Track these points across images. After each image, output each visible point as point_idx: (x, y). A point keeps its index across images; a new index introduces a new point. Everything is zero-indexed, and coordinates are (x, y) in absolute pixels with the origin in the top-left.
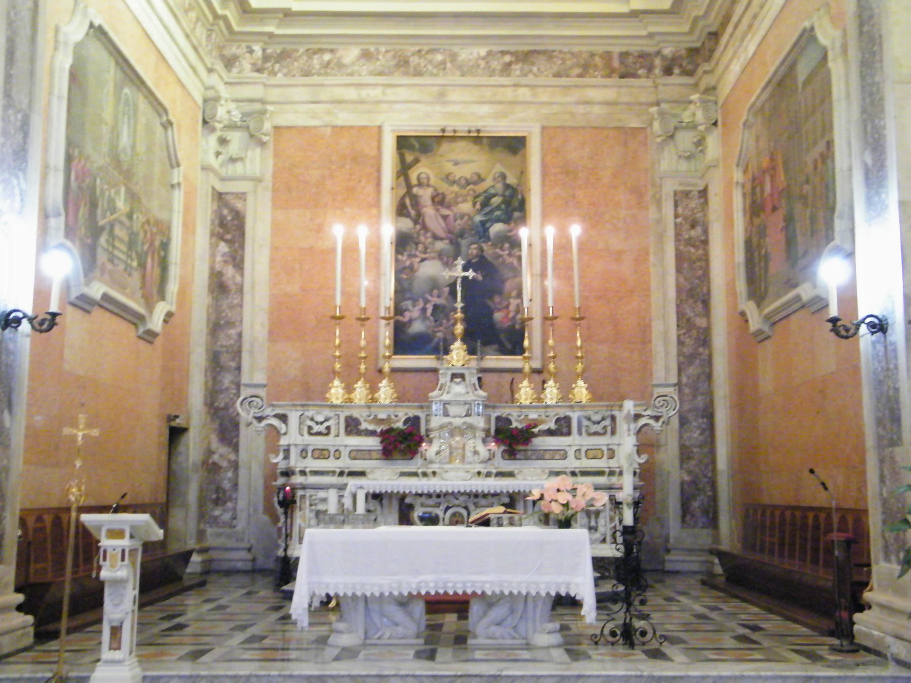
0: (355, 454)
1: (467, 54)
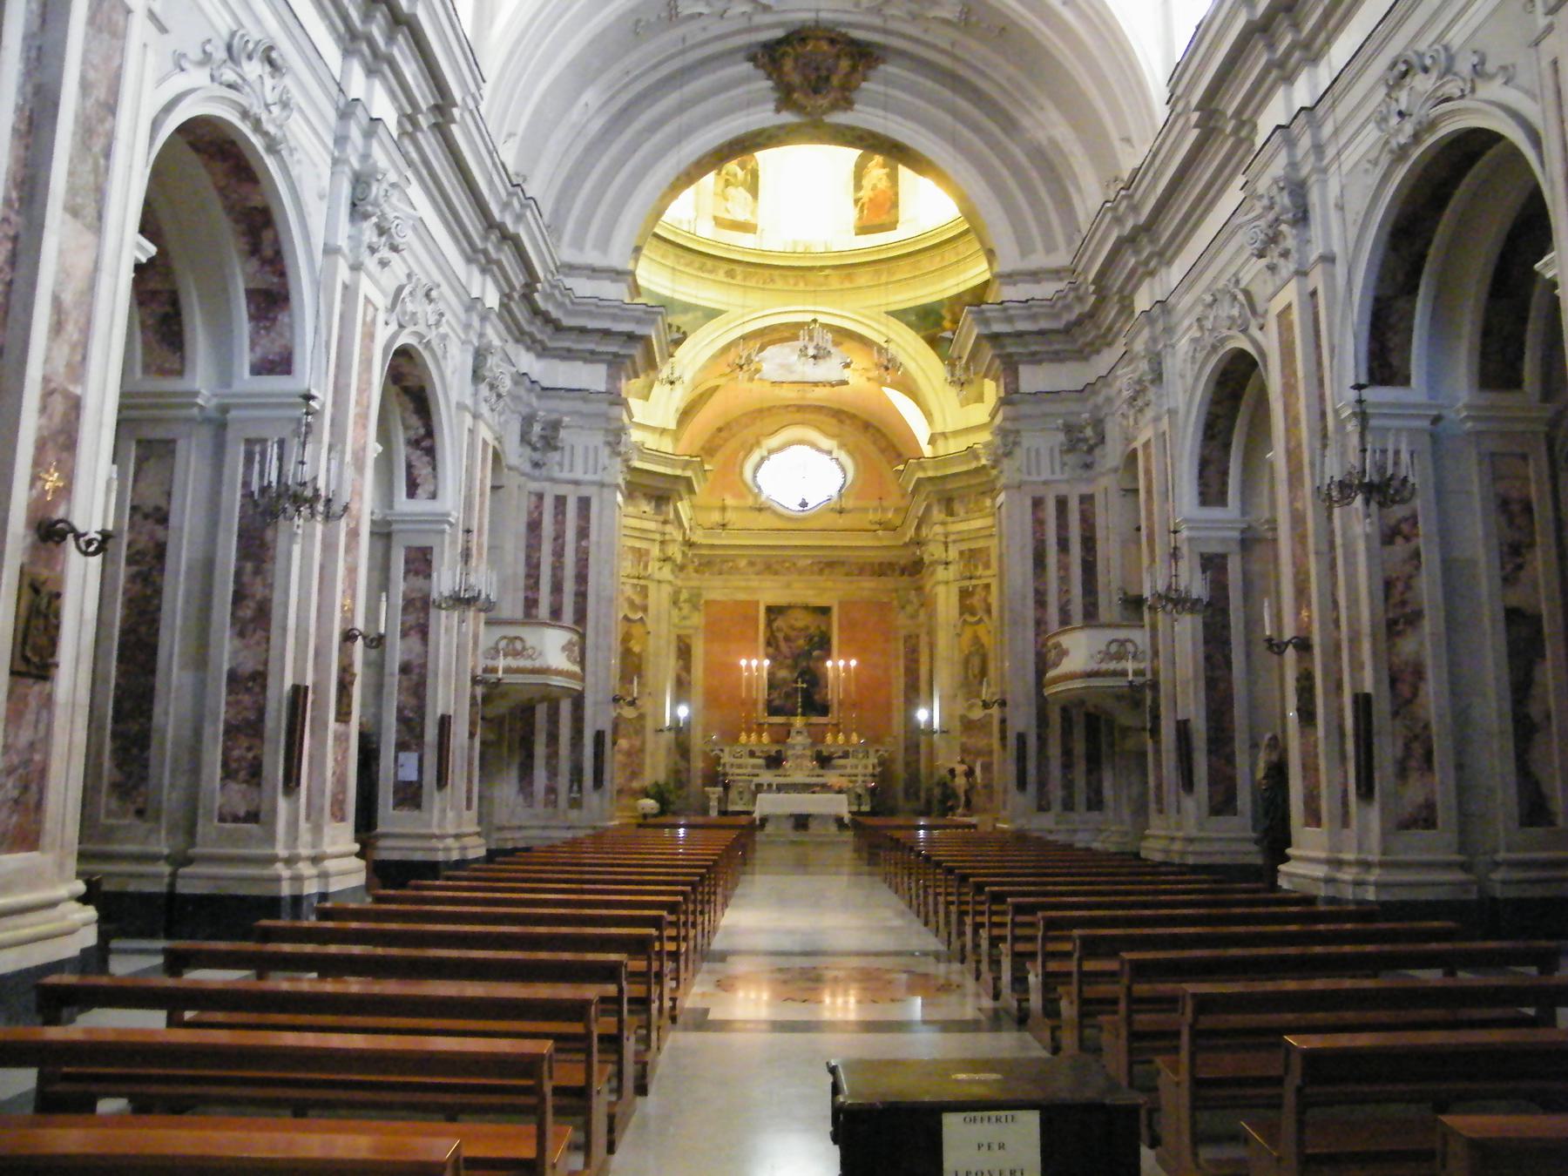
0: (754, 766)
1: (802, 563)
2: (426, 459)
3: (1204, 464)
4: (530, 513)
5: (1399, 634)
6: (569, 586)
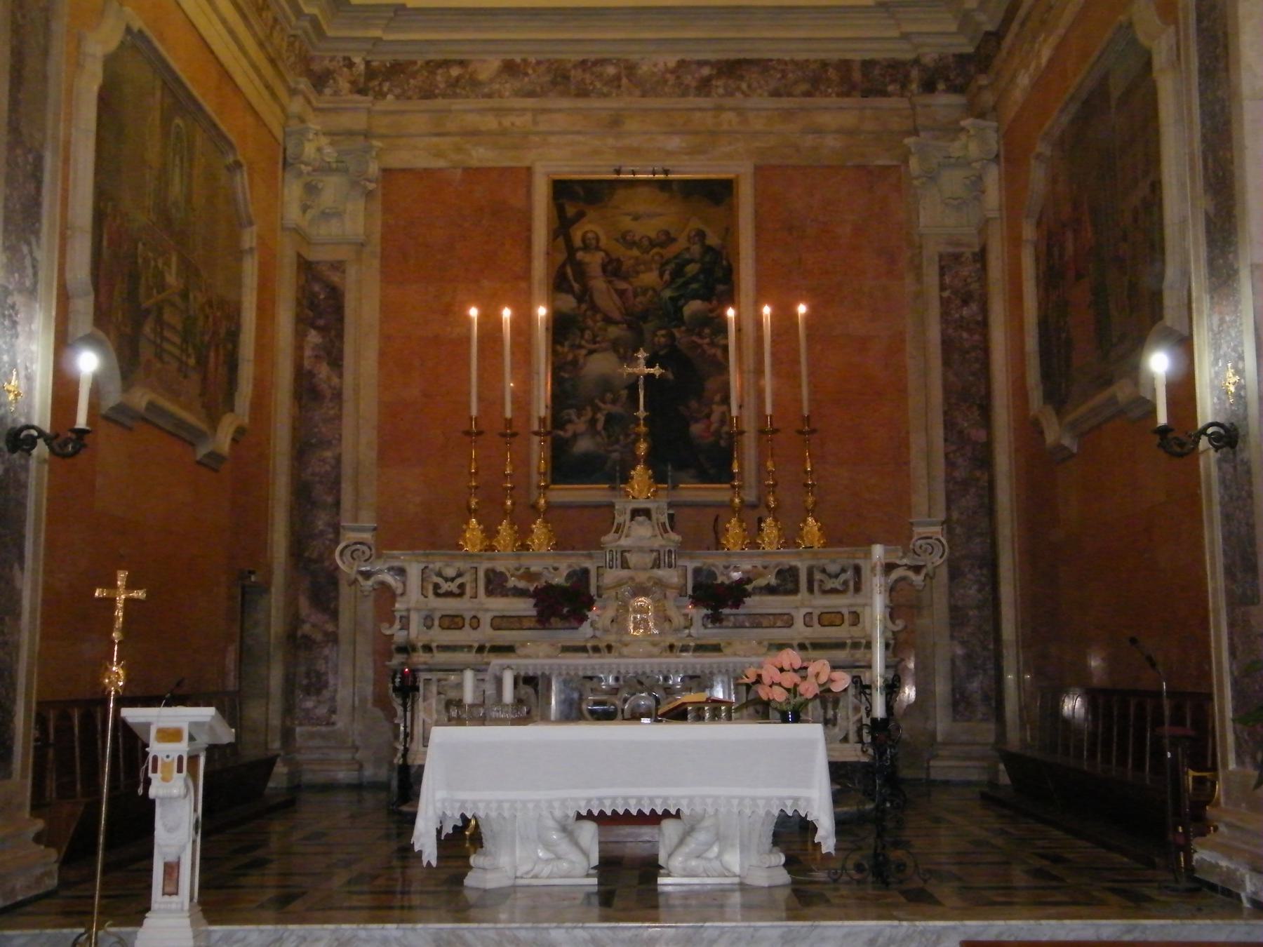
0: (501, 622)
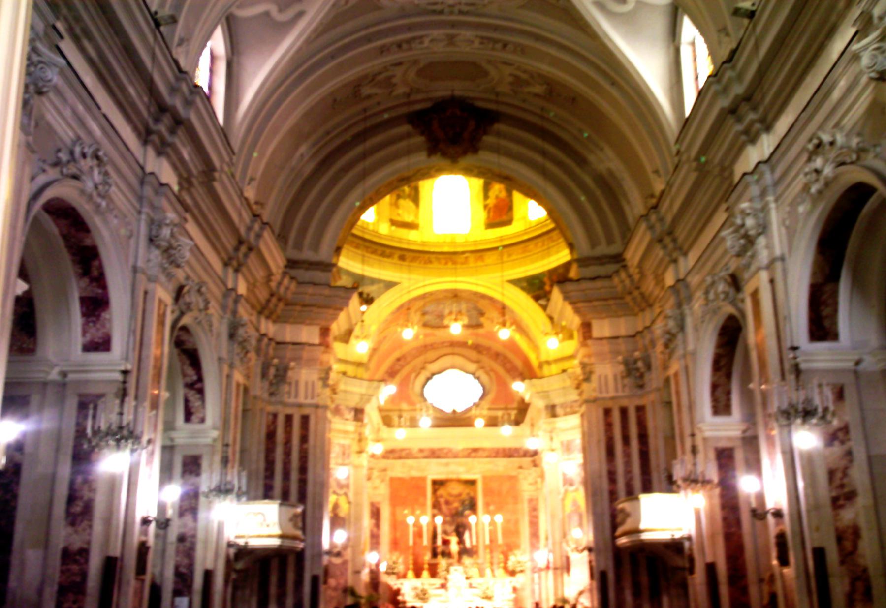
2: (198, 396)
3: (714, 387)
4: (268, 426)
5: (841, 507)
6: (295, 476)
